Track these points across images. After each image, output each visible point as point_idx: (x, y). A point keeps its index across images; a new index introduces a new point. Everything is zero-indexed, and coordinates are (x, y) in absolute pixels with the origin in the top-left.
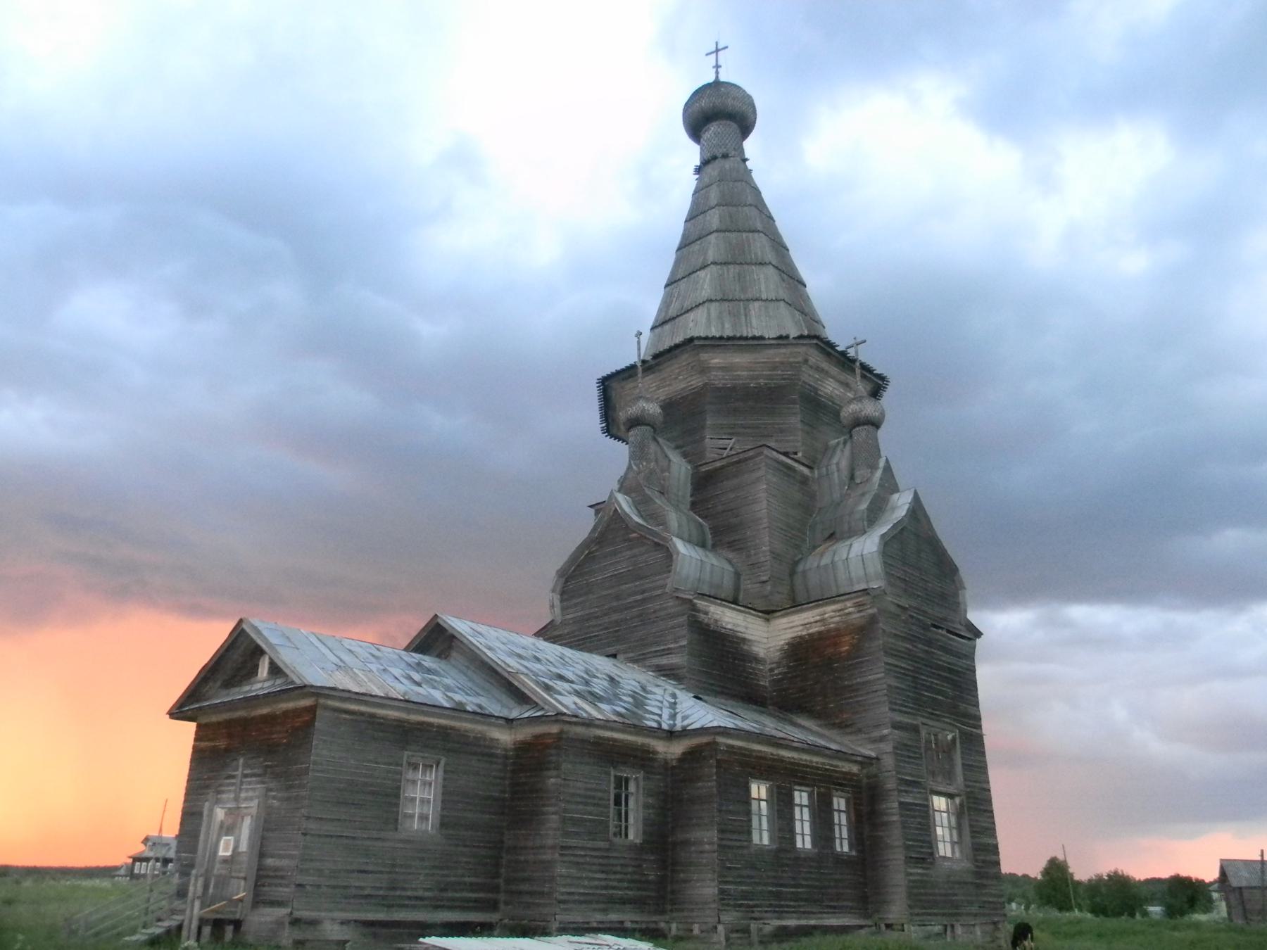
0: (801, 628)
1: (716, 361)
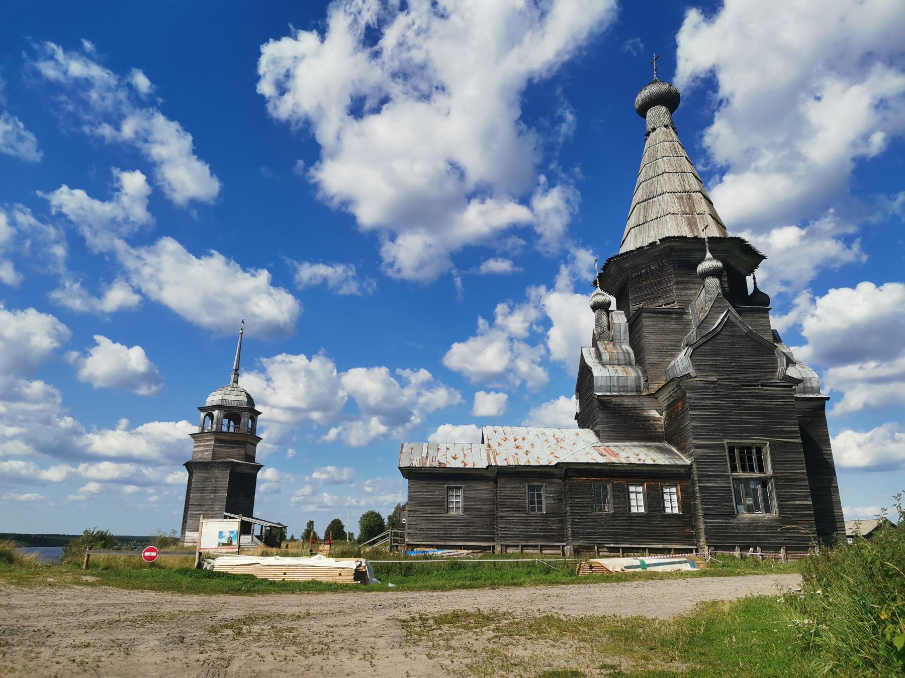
0: (667, 400)
1: (627, 265)
